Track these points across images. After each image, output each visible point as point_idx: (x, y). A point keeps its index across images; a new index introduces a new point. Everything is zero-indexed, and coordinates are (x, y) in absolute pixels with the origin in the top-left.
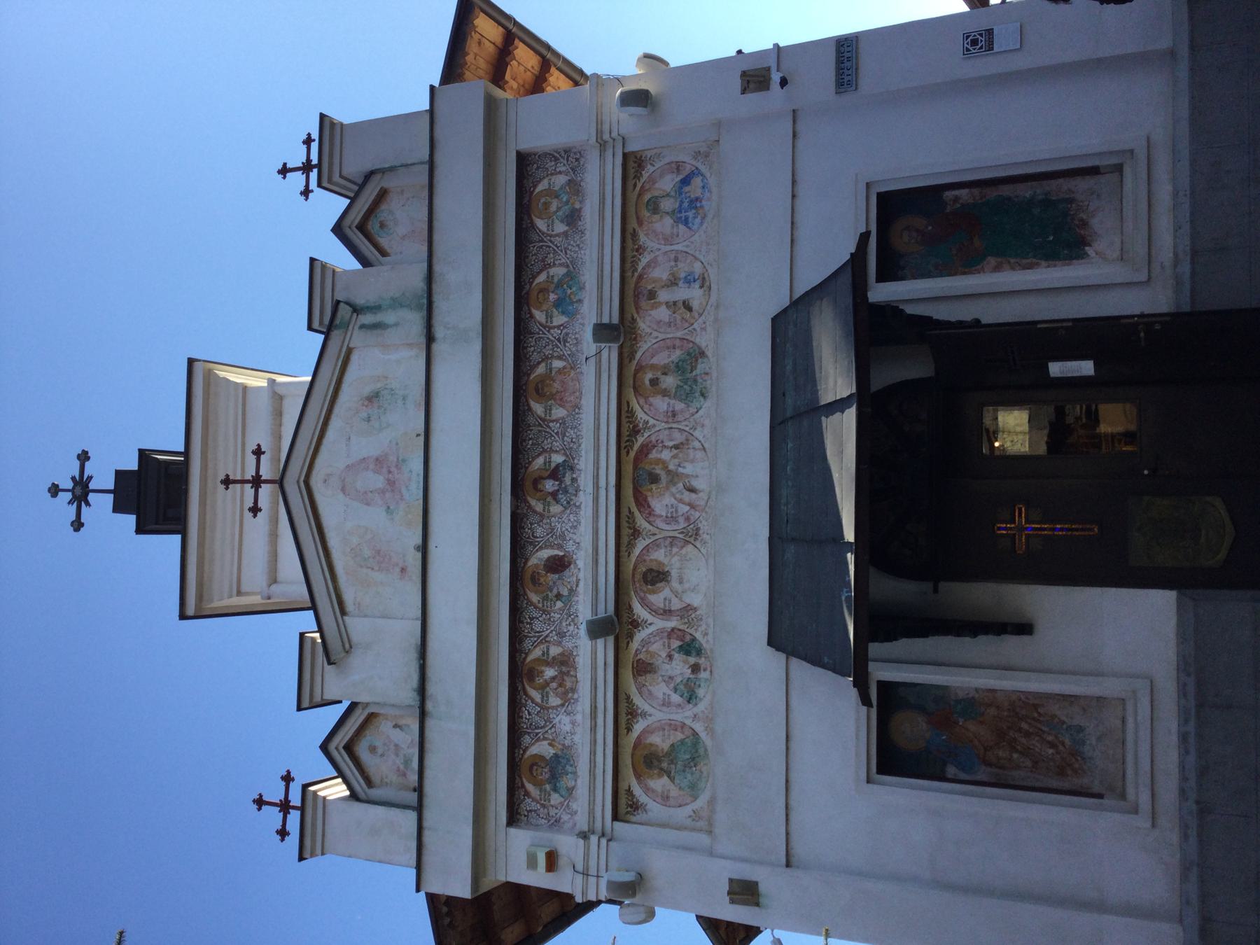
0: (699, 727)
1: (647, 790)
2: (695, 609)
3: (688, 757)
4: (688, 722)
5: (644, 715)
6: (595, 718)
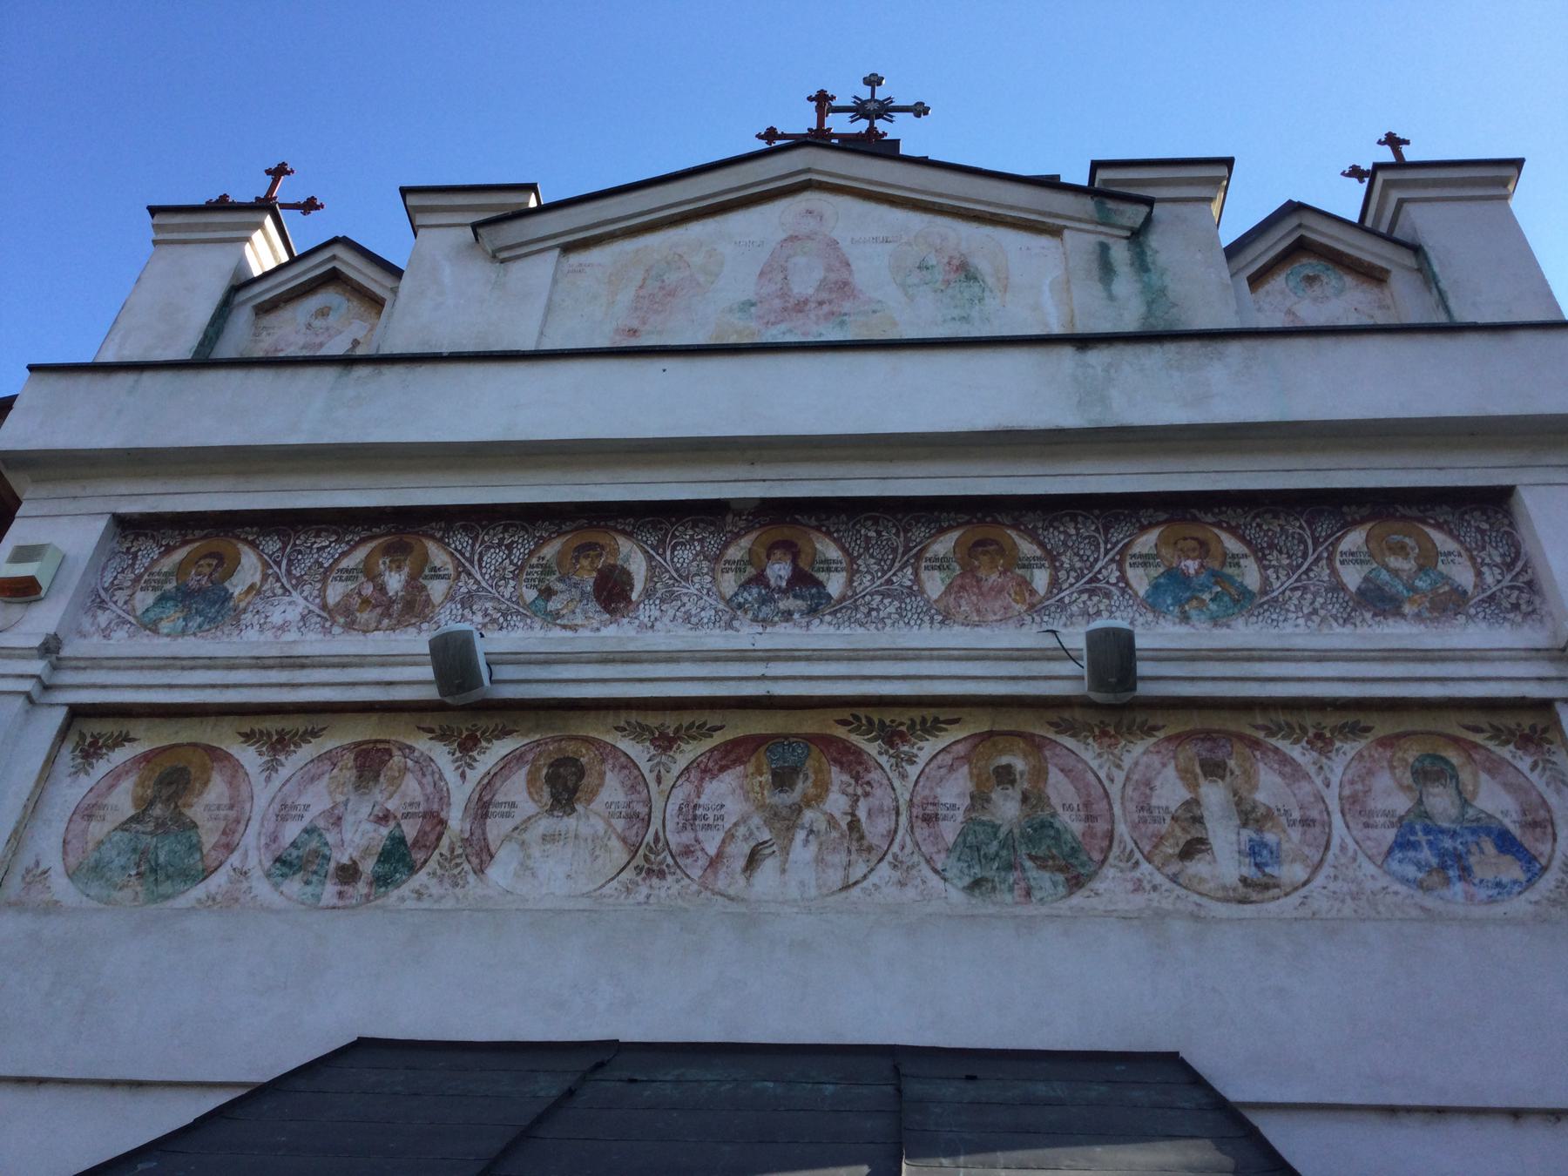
0: (218, 881)
1: (116, 776)
2: (480, 871)
3: (162, 859)
4: (235, 859)
5: (272, 767)
6: (282, 667)
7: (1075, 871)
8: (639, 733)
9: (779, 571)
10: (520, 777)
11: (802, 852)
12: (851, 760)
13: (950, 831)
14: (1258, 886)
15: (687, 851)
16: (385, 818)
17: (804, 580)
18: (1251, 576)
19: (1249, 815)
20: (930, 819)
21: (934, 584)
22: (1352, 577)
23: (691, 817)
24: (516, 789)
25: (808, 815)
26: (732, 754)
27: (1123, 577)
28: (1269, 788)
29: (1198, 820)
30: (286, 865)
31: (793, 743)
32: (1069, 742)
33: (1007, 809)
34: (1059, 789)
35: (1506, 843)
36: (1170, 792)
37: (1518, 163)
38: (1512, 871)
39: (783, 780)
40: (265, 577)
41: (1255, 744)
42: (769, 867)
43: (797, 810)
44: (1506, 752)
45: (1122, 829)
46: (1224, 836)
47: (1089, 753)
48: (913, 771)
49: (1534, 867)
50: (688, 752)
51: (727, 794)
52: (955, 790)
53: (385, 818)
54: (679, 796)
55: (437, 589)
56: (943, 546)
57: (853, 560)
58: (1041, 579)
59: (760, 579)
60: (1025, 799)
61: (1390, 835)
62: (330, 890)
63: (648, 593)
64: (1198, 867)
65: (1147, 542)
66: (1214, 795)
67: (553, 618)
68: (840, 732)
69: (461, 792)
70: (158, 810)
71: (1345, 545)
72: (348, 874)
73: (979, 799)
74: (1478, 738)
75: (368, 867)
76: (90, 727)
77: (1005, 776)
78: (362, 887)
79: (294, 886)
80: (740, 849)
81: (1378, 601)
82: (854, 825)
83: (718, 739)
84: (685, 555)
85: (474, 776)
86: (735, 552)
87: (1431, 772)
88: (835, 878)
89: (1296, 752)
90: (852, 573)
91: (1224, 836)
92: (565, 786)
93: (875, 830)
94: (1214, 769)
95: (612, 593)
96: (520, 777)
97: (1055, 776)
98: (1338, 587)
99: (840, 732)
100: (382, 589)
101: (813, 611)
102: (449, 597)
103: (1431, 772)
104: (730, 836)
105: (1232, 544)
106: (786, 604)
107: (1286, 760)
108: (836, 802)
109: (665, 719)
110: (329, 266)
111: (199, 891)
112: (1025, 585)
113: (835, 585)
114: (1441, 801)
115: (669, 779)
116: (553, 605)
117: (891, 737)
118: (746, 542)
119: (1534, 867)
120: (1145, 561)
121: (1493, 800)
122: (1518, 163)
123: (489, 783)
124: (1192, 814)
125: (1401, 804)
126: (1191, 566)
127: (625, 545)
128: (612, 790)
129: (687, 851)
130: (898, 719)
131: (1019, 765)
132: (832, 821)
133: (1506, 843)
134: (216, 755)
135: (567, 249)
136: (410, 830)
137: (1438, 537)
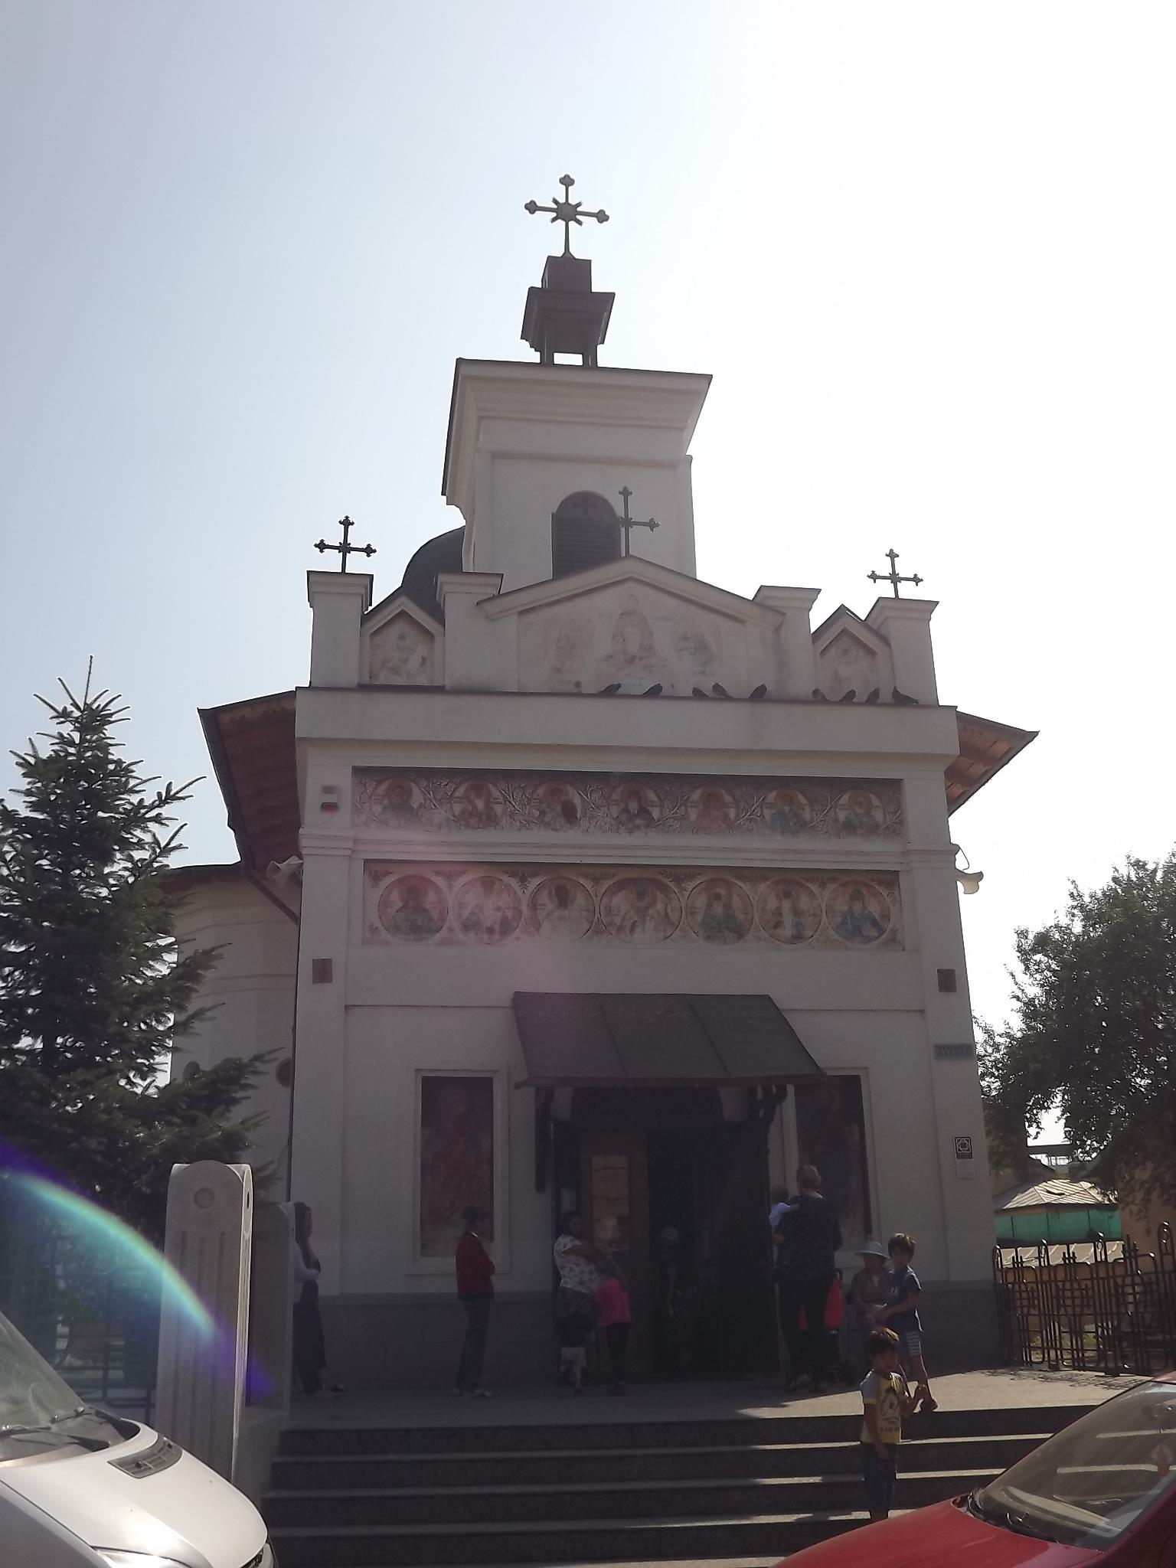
0: (443, 933)
1: (389, 888)
7: (740, 933)
8: (586, 876)
9: (633, 806)
10: (545, 893)
11: (650, 924)
12: (665, 889)
13: (699, 917)
14: (797, 938)
15: (610, 924)
16: (498, 909)
17: (644, 811)
18: (807, 815)
19: (797, 912)
20: (693, 913)
21: (693, 814)
22: (842, 816)
23: (609, 911)
24: (544, 898)
25: (651, 911)
26: (621, 885)
27: (762, 814)
28: (804, 902)
29: (781, 915)
30: (466, 927)
31: (646, 882)
32: (739, 883)
33: (718, 909)
34: (736, 902)
35: (875, 923)
36: (773, 904)
37: (819, 591)
38: (874, 933)
39: (641, 896)
40: (425, 799)
41: (801, 885)
42: (638, 930)
43: (647, 908)
44: (880, 889)
45: (756, 918)
46: (788, 919)
47: (746, 887)
48: (687, 894)
49: (882, 931)
50: (606, 884)
51: (621, 902)
52: (701, 902)
53: (498, 909)
54: (604, 901)
55: (498, 809)
56: (696, 795)
57: (661, 800)
58: (732, 813)
59: (626, 810)
60: (724, 906)
61: (839, 919)
62: (486, 937)
63: (584, 814)
64: (779, 931)
65: (772, 796)
66: (786, 905)
67: (548, 825)
68: (660, 877)
69: (525, 900)
70: (411, 903)
71: (841, 802)
72: (490, 931)
73: (709, 905)
74: (873, 884)
75: (497, 927)
76: (375, 869)
77: (718, 897)
78: (497, 936)
79: (472, 934)
80: (628, 924)
81: (849, 828)
82: (667, 915)
83: (614, 880)
84: (596, 795)
85: (528, 892)
86: (616, 796)
87: (856, 896)
88: (661, 935)
89: (814, 888)
90: (662, 807)
91: (788, 919)
92: (563, 898)
93: (674, 916)
94: (787, 895)
95: (569, 814)
96: (545, 893)
97: (735, 898)
98: (836, 820)
99: (660, 877)
100: (475, 807)
101: (648, 826)
102: (504, 813)
103: (856, 896)
104: (623, 919)
105: (803, 800)
106: (638, 822)
107: (811, 892)
108: (660, 906)
109: (597, 872)
110: (855, 1073)
111: (438, 936)
112: (726, 816)
113: (655, 813)
114: (857, 907)
115: (600, 895)
116: (547, 819)
117: (678, 880)
118: (619, 790)
119: (882, 931)
120: (771, 806)
121: (874, 908)
122: (819, 591)
123: (535, 895)
124: (778, 912)
125: (845, 908)
126: (787, 809)
127: (571, 790)
128: (580, 900)
129: (610, 924)
130: (681, 874)
131: (723, 892)
132: (659, 913)
133: (875, 923)
134: (427, 881)
135: (521, 613)
136: (509, 914)
137: (873, 797)
